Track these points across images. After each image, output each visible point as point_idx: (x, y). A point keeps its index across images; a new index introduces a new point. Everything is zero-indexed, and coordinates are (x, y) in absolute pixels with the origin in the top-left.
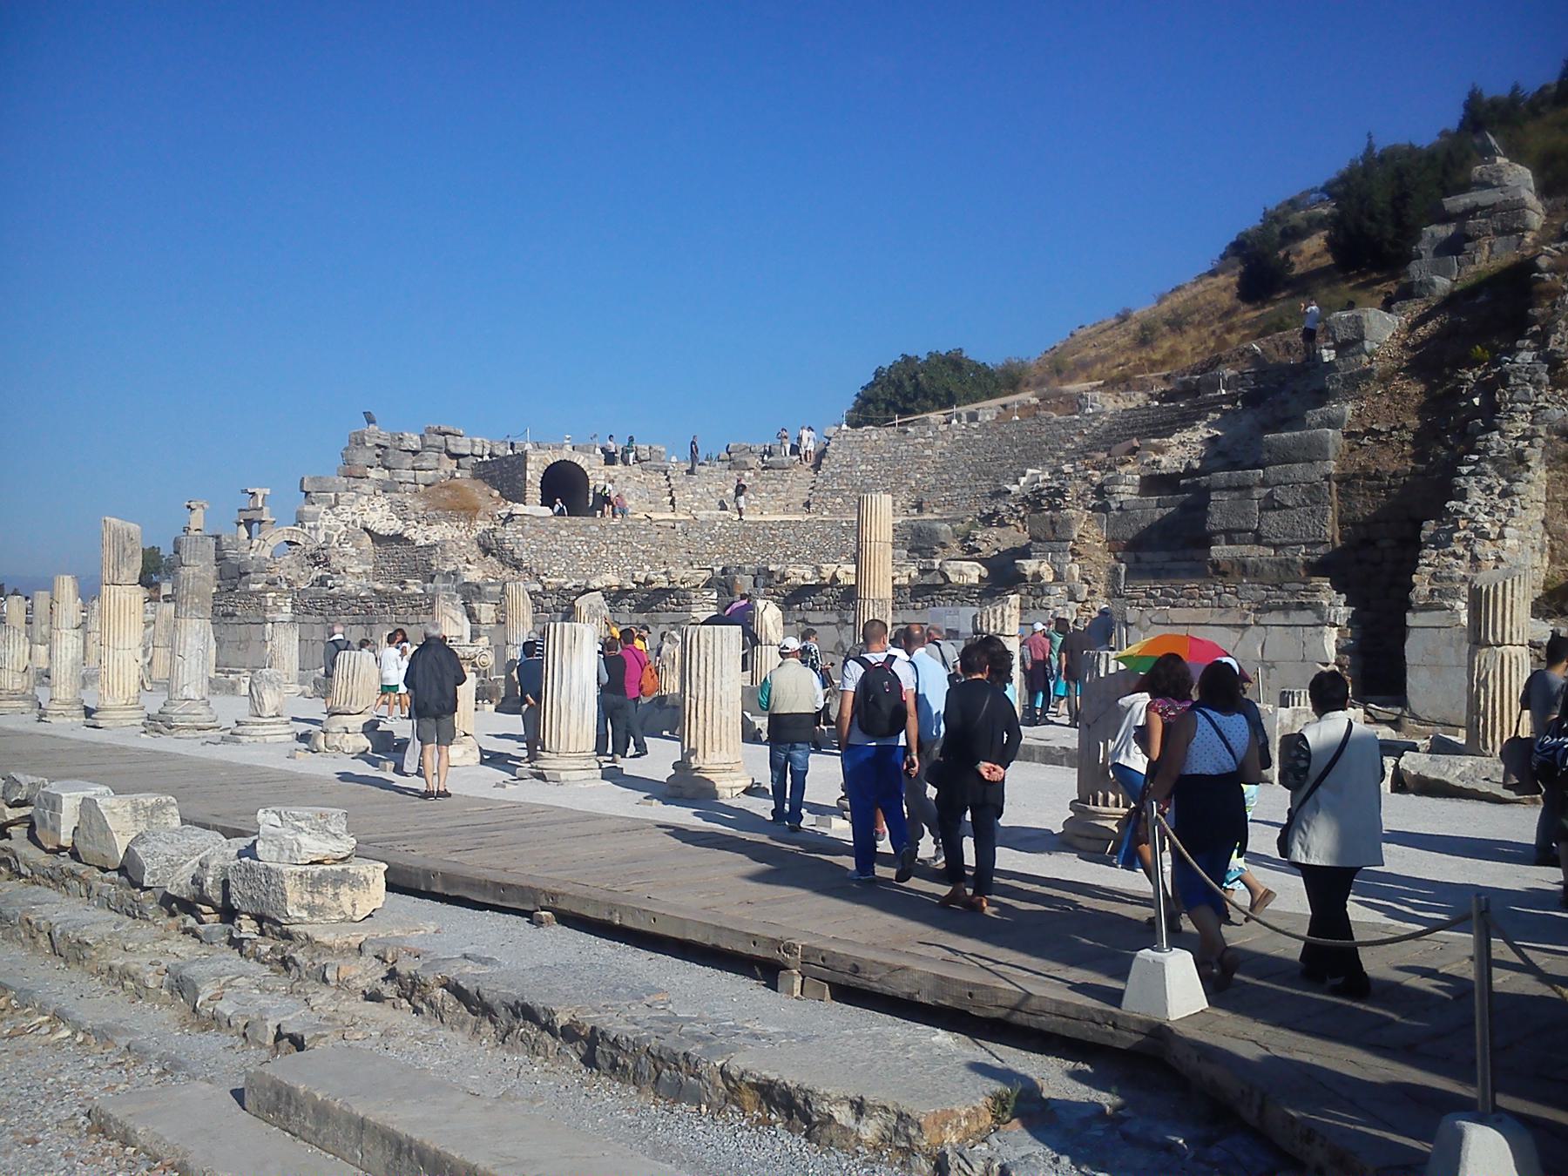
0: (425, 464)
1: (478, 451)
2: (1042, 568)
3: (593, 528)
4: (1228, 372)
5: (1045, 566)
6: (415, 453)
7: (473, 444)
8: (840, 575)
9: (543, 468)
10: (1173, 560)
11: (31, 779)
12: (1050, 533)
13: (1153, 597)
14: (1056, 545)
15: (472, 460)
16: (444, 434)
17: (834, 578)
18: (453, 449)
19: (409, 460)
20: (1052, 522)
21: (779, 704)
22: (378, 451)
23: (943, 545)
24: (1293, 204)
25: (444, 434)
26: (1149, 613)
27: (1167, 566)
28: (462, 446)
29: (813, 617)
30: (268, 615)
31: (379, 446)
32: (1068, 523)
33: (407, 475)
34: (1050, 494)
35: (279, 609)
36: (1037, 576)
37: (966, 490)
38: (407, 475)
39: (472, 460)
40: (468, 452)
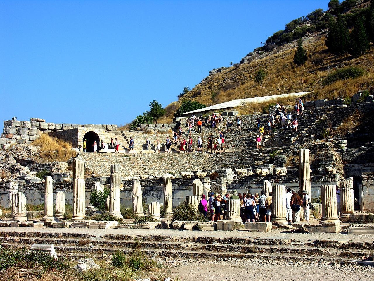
0: (33, 133)
2: (333, 170)
3: (107, 157)
6: (29, 129)
7: (49, 125)
9: (84, 134)
10: (365, 166)
11: (110, 228)
13: (371, 177)
14: (328, 162)
15: (48, 131)
17: (261, 173)
18: (43, 127)
19: (27, 132)
22: (17, 128)
23: (285, 162)
24: (296, 22)
26: (370, 182)
28: (44, 126)
30: (11, 191)
31: (17, 126)
32: (331, 156)
33: (27, 137)
34: (319, 146)
36: (332, 172)
37: (238, 141)
38: (27, 137)
39: (48, 131)
40: (47, 128)
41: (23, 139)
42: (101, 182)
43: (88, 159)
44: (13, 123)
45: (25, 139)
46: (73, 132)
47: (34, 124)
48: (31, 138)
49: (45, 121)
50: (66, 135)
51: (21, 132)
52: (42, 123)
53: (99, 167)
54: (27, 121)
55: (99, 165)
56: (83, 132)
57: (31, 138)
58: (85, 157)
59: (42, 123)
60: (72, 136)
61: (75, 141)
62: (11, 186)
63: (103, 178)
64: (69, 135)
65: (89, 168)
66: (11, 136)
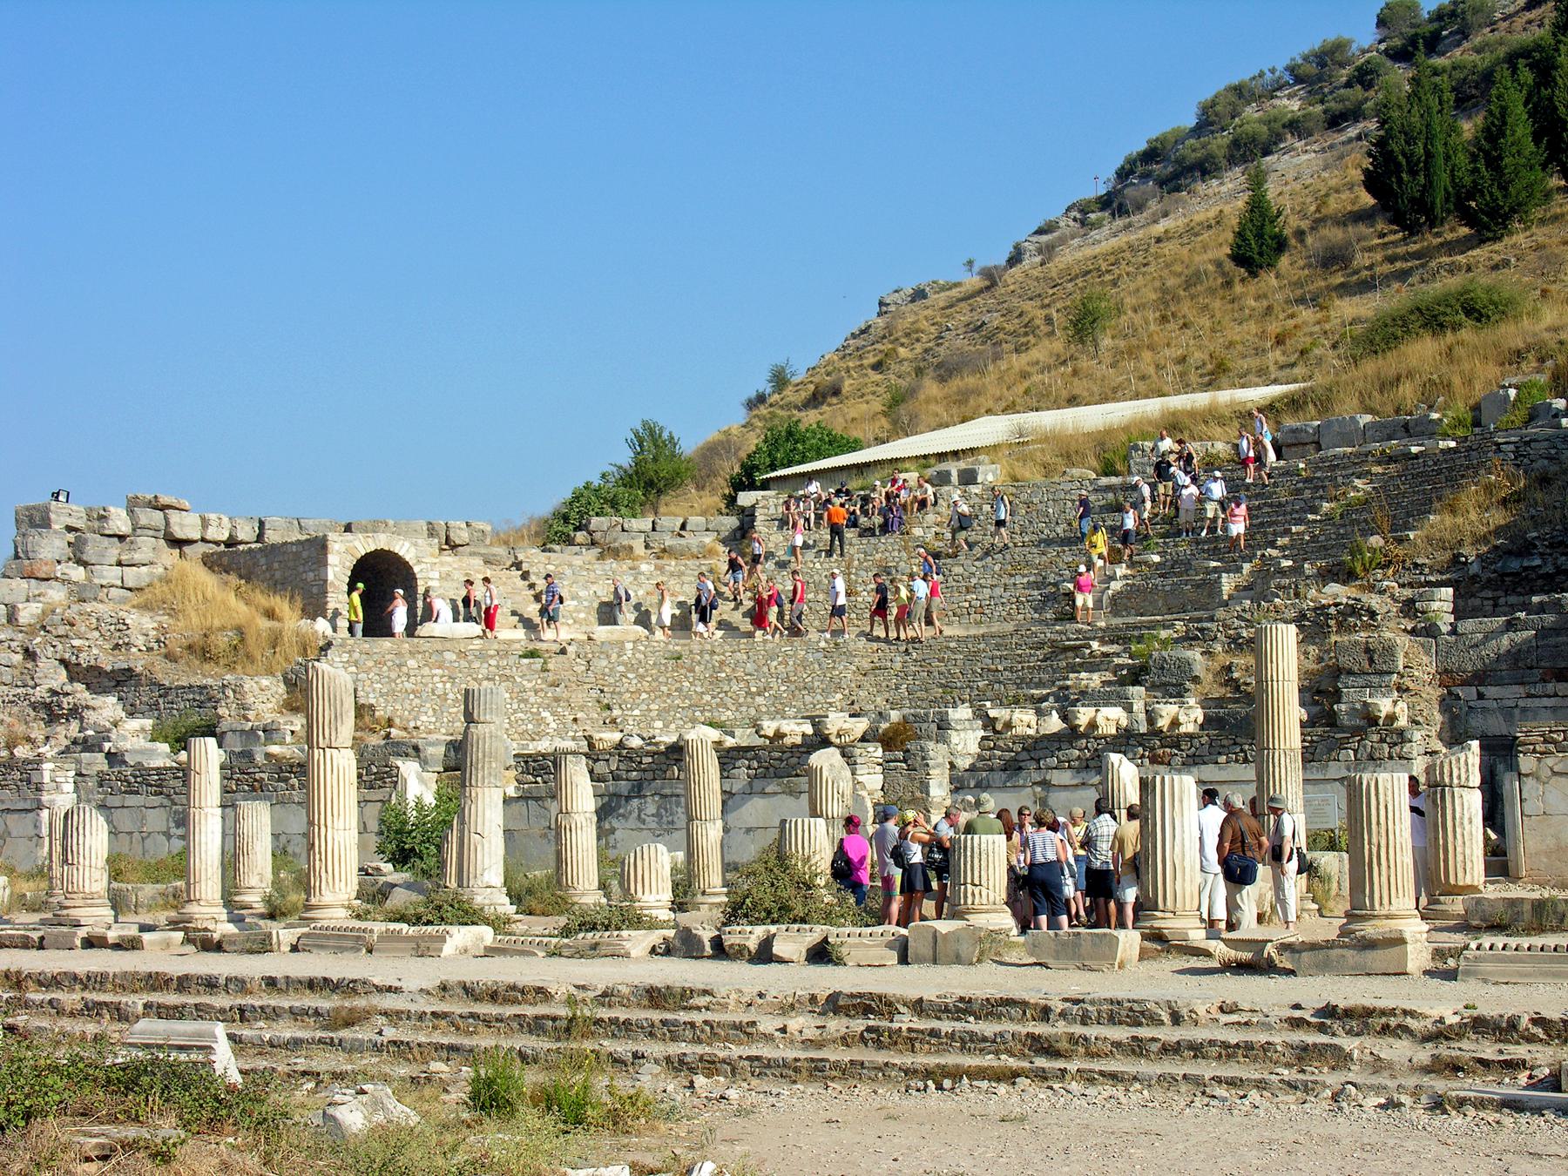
0: (137, 557)
1: (212, 534)
2: (1397, 710)
4: (1245, 444)
5: (1402, 705)
6: (121, 538)
7: (205, 523)
8: (1100, 720)
9: (350, 563)
10: (1529, 696)
12: (1366, 664)
13: (1554, 742)
14: (1375, 679)
15: (201, 548)
16: (163, 508)
17: (1093, 725)
18: (179, 534)
19: (114, 551)
20: (1368, 650)
21: (165, 816)
22: (71, 537)
25: (163, 508)
26: (1550, 761)
27: (1521, 703)
28: (186, 525)
29: (1057, 777)
30: (45, 798)
31: (70, 529)
33: (111, 574)
35: (58, 788)
37: (999, 591)
38: (111, 574)
40: (197, 536)
41: (96, 581)
42: (424, 763)
43: (370, 664)
44: (53, 516)
45: (104, 582)
46: (305, 554)
47: (143, 521)
48: (132, 576)
49: (187, 505)
50: (276, 565)
51: (90, 554)
52: (174, 517)
53: (417, 701)
54: (112, 509)
55: (413, 692)
56: (347, 551)
57: (132, 576)
58: (356, 655)
59: (174, 517)
60: (301, 569)
61: (315, 590)
62: (46, 779)
63: (432, 744)
64: (291, 564)
65: (373, 701)
66: (44, 568)
